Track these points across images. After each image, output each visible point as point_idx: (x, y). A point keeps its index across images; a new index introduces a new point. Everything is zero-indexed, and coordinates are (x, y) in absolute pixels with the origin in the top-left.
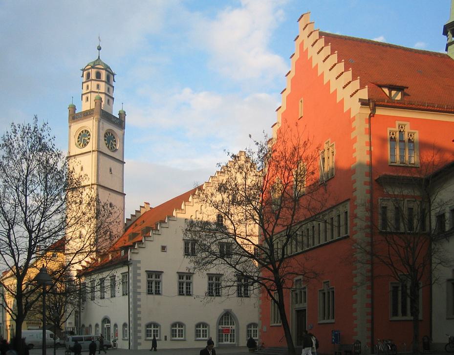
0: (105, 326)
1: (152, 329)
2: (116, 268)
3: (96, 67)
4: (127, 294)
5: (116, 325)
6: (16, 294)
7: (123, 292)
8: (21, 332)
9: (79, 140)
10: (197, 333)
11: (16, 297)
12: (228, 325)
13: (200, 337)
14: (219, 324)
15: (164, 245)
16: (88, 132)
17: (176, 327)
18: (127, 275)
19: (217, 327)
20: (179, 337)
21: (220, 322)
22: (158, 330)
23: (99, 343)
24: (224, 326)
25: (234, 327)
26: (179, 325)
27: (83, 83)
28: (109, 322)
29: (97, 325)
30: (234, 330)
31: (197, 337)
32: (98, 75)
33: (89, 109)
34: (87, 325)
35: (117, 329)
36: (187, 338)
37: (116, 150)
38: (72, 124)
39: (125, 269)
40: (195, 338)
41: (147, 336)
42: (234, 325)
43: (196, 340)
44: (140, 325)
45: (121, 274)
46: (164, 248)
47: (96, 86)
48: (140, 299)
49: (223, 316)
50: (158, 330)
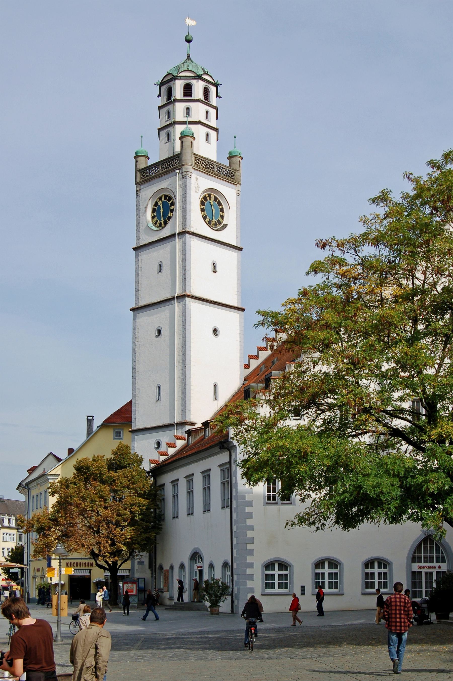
1: (376, 570)
3: (181, 74)
5: (211, 566)
6: (408, 485)
9: (155, 214)
10: (368, 579)
12: (432, 562)
13: (273, 587)
16: (170, 198)
19: (409, 567)
20: (280, 587)
22: (386, 573)
23: (221, 604)
24: (421, 565)
26: (329, 563)
27: (160, 108)
29: (182, 566)
31: (367, 587)
32: (188, 90)
33: (172, 155)
34: (166, 567)
35: (213, 573)
36: (345, 591)
37: (225, 226)
38: (142, 187)
39: (224, 457)
40: (363, 589)
41: (267, 586)
42: (444, 562)
43: (363, 594)
44: (251, 565)
45: (220, 466)
47: (192, 112)
48: (253, 551)
49: (419, 546)
50: (386, 573)
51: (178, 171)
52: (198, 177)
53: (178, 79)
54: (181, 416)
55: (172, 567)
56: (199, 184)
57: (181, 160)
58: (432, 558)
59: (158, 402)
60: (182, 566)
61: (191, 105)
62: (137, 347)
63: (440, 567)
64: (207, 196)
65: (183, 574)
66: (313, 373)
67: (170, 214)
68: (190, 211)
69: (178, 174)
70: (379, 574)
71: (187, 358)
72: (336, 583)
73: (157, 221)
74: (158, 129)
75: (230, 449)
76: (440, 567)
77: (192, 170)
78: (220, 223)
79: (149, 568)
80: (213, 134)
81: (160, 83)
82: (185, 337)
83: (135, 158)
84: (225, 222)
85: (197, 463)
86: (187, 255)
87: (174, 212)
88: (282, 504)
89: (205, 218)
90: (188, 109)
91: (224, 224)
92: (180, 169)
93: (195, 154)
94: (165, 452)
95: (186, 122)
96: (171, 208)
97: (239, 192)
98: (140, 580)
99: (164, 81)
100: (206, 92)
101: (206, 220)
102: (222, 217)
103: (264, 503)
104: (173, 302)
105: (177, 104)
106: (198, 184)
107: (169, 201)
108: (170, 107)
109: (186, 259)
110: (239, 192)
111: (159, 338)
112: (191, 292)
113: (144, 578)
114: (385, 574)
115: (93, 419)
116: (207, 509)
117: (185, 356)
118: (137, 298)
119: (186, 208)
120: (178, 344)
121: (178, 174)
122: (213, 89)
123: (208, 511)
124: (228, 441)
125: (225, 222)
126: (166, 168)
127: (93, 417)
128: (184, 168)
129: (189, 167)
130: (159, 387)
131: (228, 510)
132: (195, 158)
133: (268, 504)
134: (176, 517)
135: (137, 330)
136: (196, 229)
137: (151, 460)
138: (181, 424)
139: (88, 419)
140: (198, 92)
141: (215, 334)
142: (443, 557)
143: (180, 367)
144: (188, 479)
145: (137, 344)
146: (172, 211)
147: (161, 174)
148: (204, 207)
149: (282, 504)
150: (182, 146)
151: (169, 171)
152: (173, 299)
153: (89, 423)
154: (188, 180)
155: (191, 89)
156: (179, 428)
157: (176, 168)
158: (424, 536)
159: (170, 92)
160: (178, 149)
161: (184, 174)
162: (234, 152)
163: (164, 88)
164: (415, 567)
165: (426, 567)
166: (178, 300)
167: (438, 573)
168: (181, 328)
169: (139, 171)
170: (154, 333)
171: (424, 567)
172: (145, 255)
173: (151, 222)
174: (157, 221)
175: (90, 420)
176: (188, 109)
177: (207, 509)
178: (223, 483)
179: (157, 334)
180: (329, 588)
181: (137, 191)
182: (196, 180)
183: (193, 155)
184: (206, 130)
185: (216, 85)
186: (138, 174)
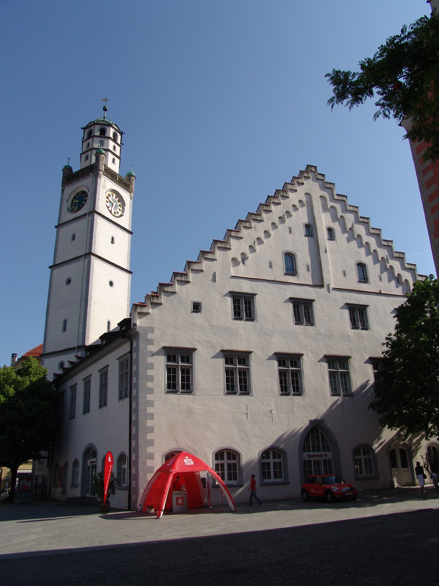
0: (89, 464)
2: (66, 355)
4: (126, 396)
7: (121, 392)
8: (138, 499)
11: (58, 225)
12: (319, 451)
14: (304, 451)
15: (197, 300)
17: (360, 454)
18: (128, 361)
20: (275, 477)
21: (304, 447)
24: (311, 453)
25: (330, 455)
28: (95, 454)
29: (76, 462)
30: (330, 461)
31: (265, 478)
34: (62, 464)
42: (329, 450)
46: (197, 307)
49: (308, 435)
52: (80, 486)
55: (66, 464)
56: (106, 184)
58: (319, 446)
60: (76, 462)
63: (326, 456)
65: (77, 470)
67: (84, 203)
70: (275, 464)
72: (235, 474)
74: (80, 154)
75: (131, 338)
76: (326, 456)
77: (102, 174)
79: (47, 467)
85: (95, 364)
96: (85, 199)
98: (39, 477)
99: (88, 126)
100: (115, 135)
106: (105, 184)
107: (84, 194)
108: (90, 141)
111: (68, 286)
112: (95, 253)
113: (43, 476)
114: (280, 463)
116: (103, 403)
131: (127, 400)
132: (105, 168)
134: (73, 417)
136: (102, 212)
138: (79, 347)
139: (12, 356)
142: (328, 446)
144: (86, 381)
146: (86, 200)
153: (13, 359)
154: (99, 180)
159: (90, 133)
160: (93, 161)
163: (86, 131)
164: (305, 455)
165: (315, 456)
167: (325, 461)
171: (312, 456)
175: (14, 356)
179: (68, 283)
180: (274, 478)
182: (104, 182)
183: (103, 166)
185: (121, 134)
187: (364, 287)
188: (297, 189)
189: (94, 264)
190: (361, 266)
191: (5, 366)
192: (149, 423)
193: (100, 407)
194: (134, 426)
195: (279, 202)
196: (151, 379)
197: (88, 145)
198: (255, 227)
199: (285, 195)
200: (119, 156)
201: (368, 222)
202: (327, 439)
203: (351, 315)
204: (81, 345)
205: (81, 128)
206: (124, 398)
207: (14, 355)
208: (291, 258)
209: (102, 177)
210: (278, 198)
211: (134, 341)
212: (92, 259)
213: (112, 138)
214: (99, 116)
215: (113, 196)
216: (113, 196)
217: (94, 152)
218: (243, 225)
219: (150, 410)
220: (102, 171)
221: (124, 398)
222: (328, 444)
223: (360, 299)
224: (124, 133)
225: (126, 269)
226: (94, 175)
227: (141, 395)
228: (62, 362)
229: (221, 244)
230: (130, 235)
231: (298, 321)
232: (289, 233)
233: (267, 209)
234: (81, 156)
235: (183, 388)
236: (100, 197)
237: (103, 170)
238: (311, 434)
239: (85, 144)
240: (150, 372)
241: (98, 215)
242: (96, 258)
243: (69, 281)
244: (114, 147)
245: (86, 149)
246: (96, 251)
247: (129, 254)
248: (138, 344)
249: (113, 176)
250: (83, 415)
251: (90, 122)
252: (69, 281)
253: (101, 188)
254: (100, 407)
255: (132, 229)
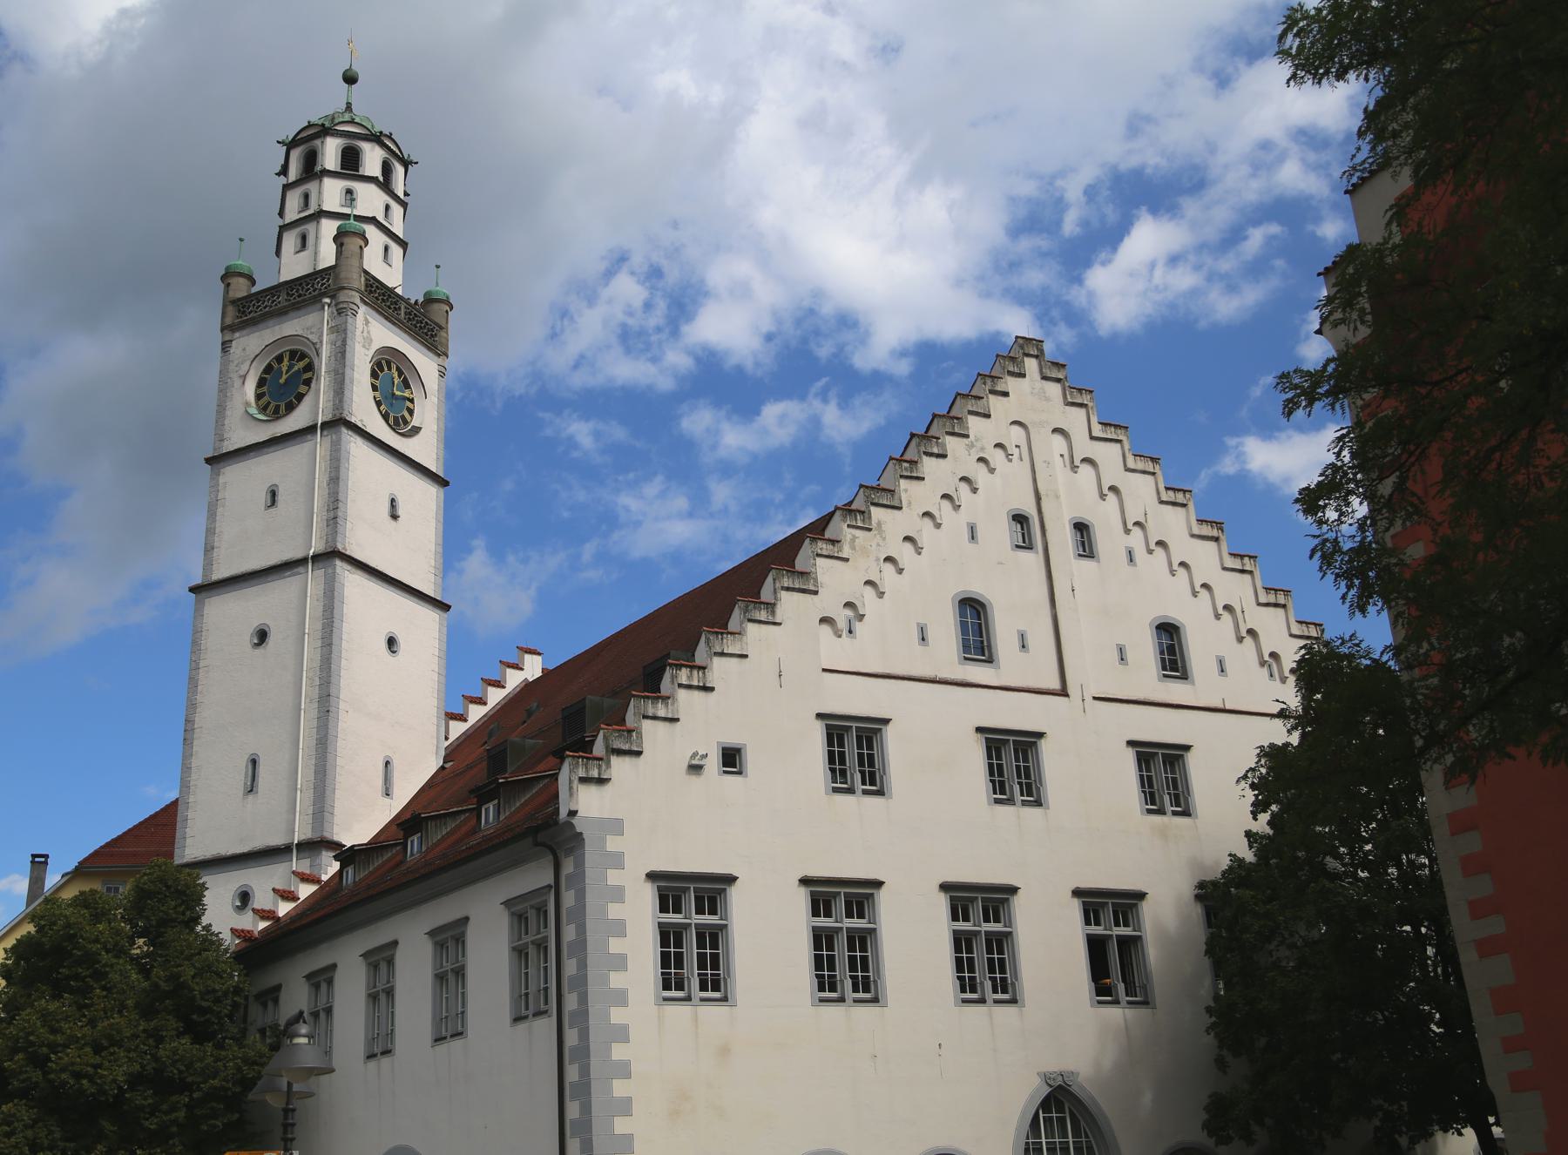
9: (265, 389)
32: (351, 159)
37: (416, 431)
38: (237, 335)
49: (1036, 1116)
51: (327, 300)
53: (332, 135)
54: (310, 826)
57: (337, 277)
59: (251, 797)
61: (359, 187)
62: (201, 671)
64: (384, 362)
66: (61, 1027)
67: (302, 389)
68: (352, 382)
69: (326, 307)
71: (333, 691)
73: (269, 403)
78: (406, 422)
80: (396, 250)
81: (290, 142)
82: (330, 645)
83: (223, 278)
84: (415, 422)
86: (342, 470)
87: (313, 385)
88: (703, 1000)
89: (378, 404)
90: (349, 192)
91: (413, 427)
92: (332, 297)
93: (366, 272)
94: (269, 911)
95: (349, 215)
97: (443, 370)
100: (387, 169)
101: (382, 408)
102: (411, 412)
103: (657, 996)
104: (301, 569)
105: (328, 182)
108: (312, 187)
109: (338, 478)
110: (443, 370)
115: (46, 863)
116: (449, 1027)
117: (328, 687)
118: (208, 565)
119: (343, 374)
120: (311, 660)
121: (326, 307)
122: (399, 170)
123: (383, 1053)
124: (556, 823)
125: (415, 422)
126: (300, 296)
127: (46, 856)
128: (342, 296)
129: (354, 293)
130: (254, 762)
131: (546, 1026)
132: (366, 279)
133: (665, 999)
135: (203, 633)
137: (236, 930)
138: (312, 846)
139: (33, 862)
140: (372, 160)
141: (390, 648)
143: (314, 713)
145: (201, 665)
146: (308, 382)
147: (285, 307)
148: (377, 383)
149: (703, 1000)
150: (339, 254)
151: (304, 301)
152: (302, 562)
155: (358, 157)
156: (302, 855)
157: (324, 295)
158: (1046, 1090)
159: (311, 159)
161: (341, 306)
162: (437, 292)
166: (316, 564)
168: (319, 626)
169: (234, 302)
170: (248, 638)
172: (232, 474)
173: (253, 404)
174: (269, 403)
175: (39, 863)
176: (349, 192)
177: (449, 1027)
178: (520, 952)
181: (223, 344)
183: (362, 275)
184: (385, 239)
185: (406, 164)
186: (230, 309)
187: (1176, 691)
188: (989, 411)
189: (344, 585)
190: (1168, 632)
191: (210, 925)
192: (620, 1088)
193: (436, 1040)
194: (573, 1098)
195: (941, 452)
196: (620, 963)
197: (306, 197)
198: (879, 524)
199: (956, 430)
200: (402, 237)
201: (1185, 502)
202: (1087, 1130)
203: (1149, 788)
204: (310, 837)
205: (278, 142)
206: (531, 1016)
207: (37, 859)
208: (975, 612)
209: (359, 311)
210: (940, 441)
211: (563, 857)
212: (338, 570)
213: (381, 179)
214: (326, 101)
215: (390, 369)
216: (390, 369)
217: (329, 228)
218: (848, 522)
219: (618, 1052)
220: (358, 291)
221: (531, 1016)
222: (1090, 1141)
223: (1162, 728)
224: (416, 163)
225: (432, 596)
226: (334, 303)
227: (594, 1007)
228: (245, 889)
229: (790, 579)
230: (442, 490)
231: (999, 789)
232: (970, 542)
233: (909, 474)
234: (279, 233)
235: (703, 988)
236: (356, 375)
237: (363, 289)
238: (1043, 1113)
239: (294, 200)
240: (615, 946)
241: (350, 433)
242: (349, 567)
243: (262, 636)
244: (387, 208)
245: (300, 212)
246: (347, 545)
247: (440, 549)
248: (580, 864)
249: (376, 298)
250: (365, 1063)
251: (309, 122)
252: (262, 636)
253: (357, 344)
254: (436, 1040)
255: (445, 472)
